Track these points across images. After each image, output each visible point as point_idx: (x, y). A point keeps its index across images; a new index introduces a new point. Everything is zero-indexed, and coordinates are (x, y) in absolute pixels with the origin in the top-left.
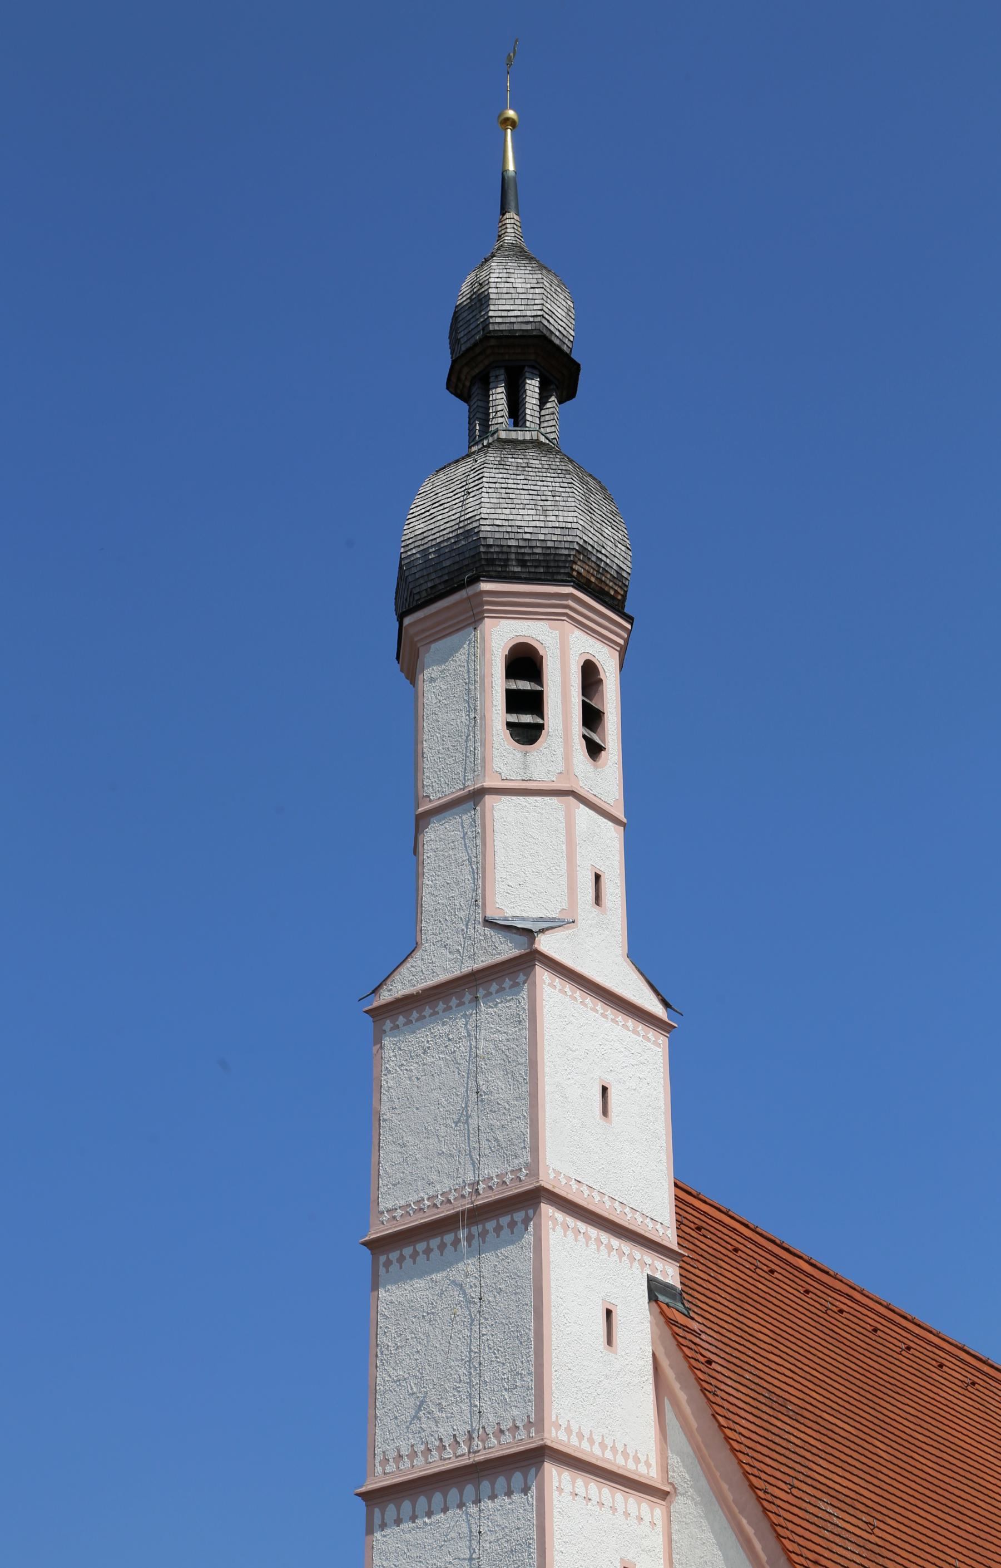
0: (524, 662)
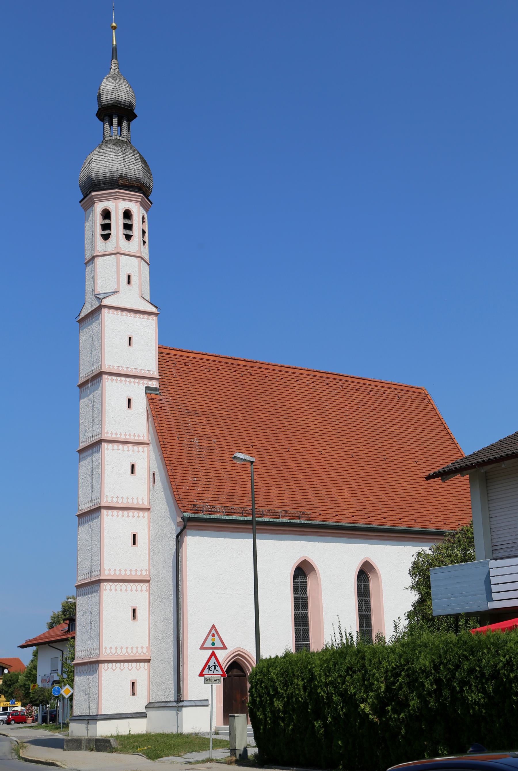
0: (106, 214)
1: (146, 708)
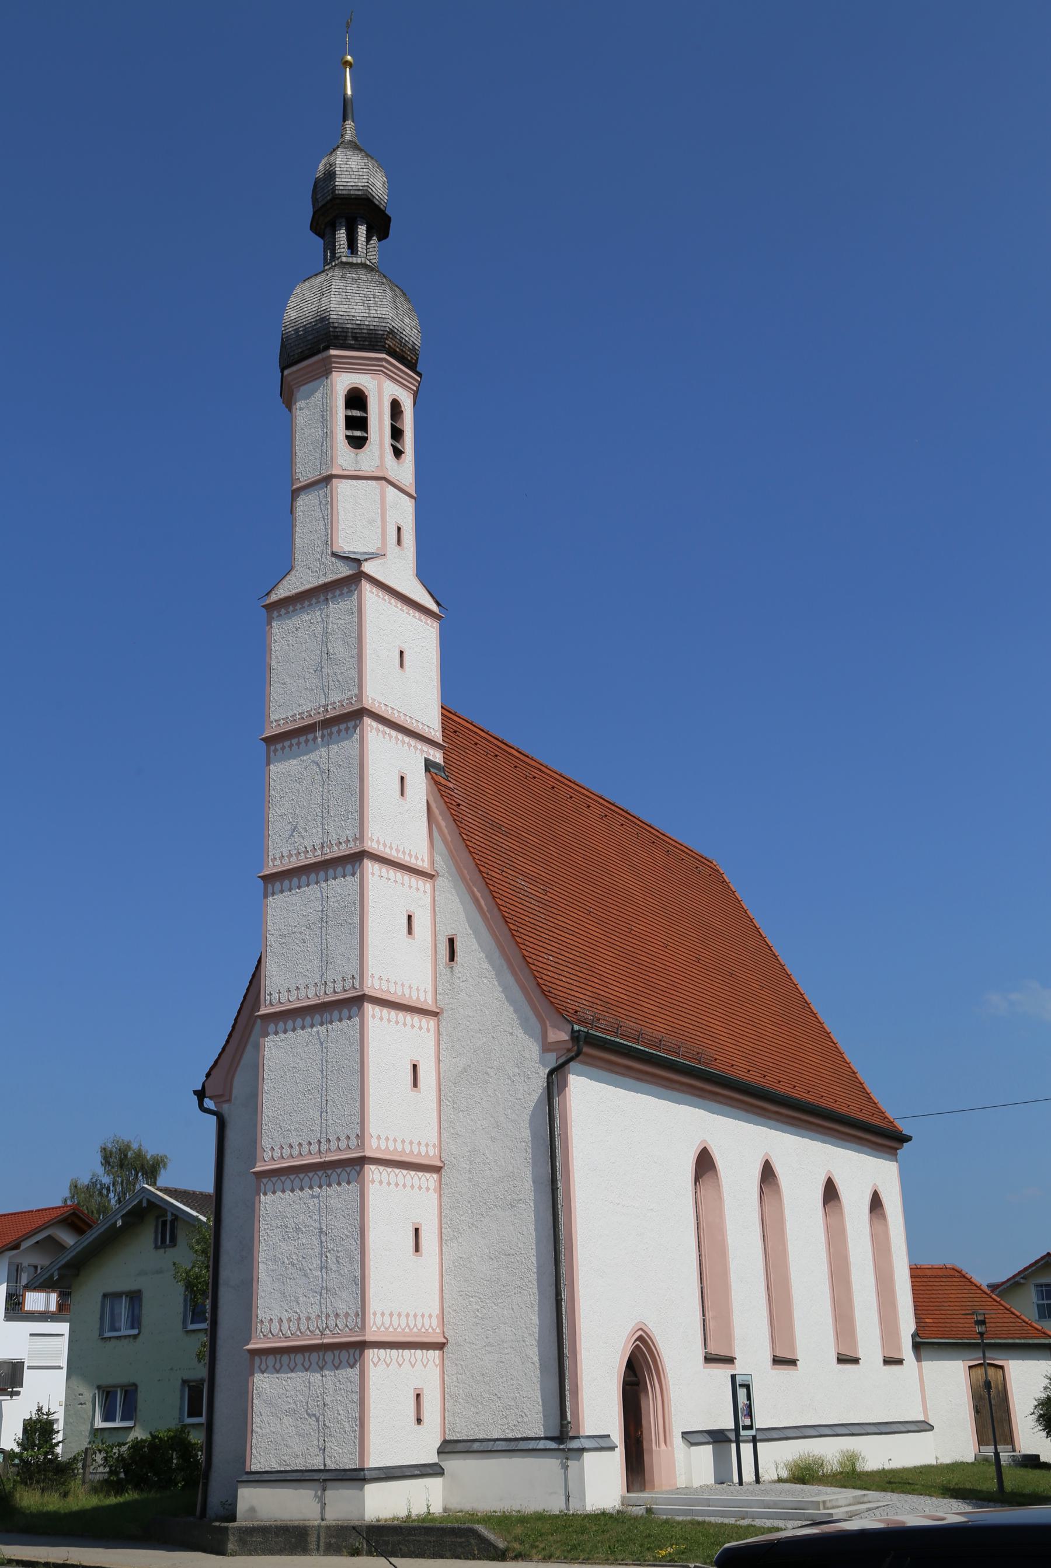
0: (356, 399)
1: (439, 1453)
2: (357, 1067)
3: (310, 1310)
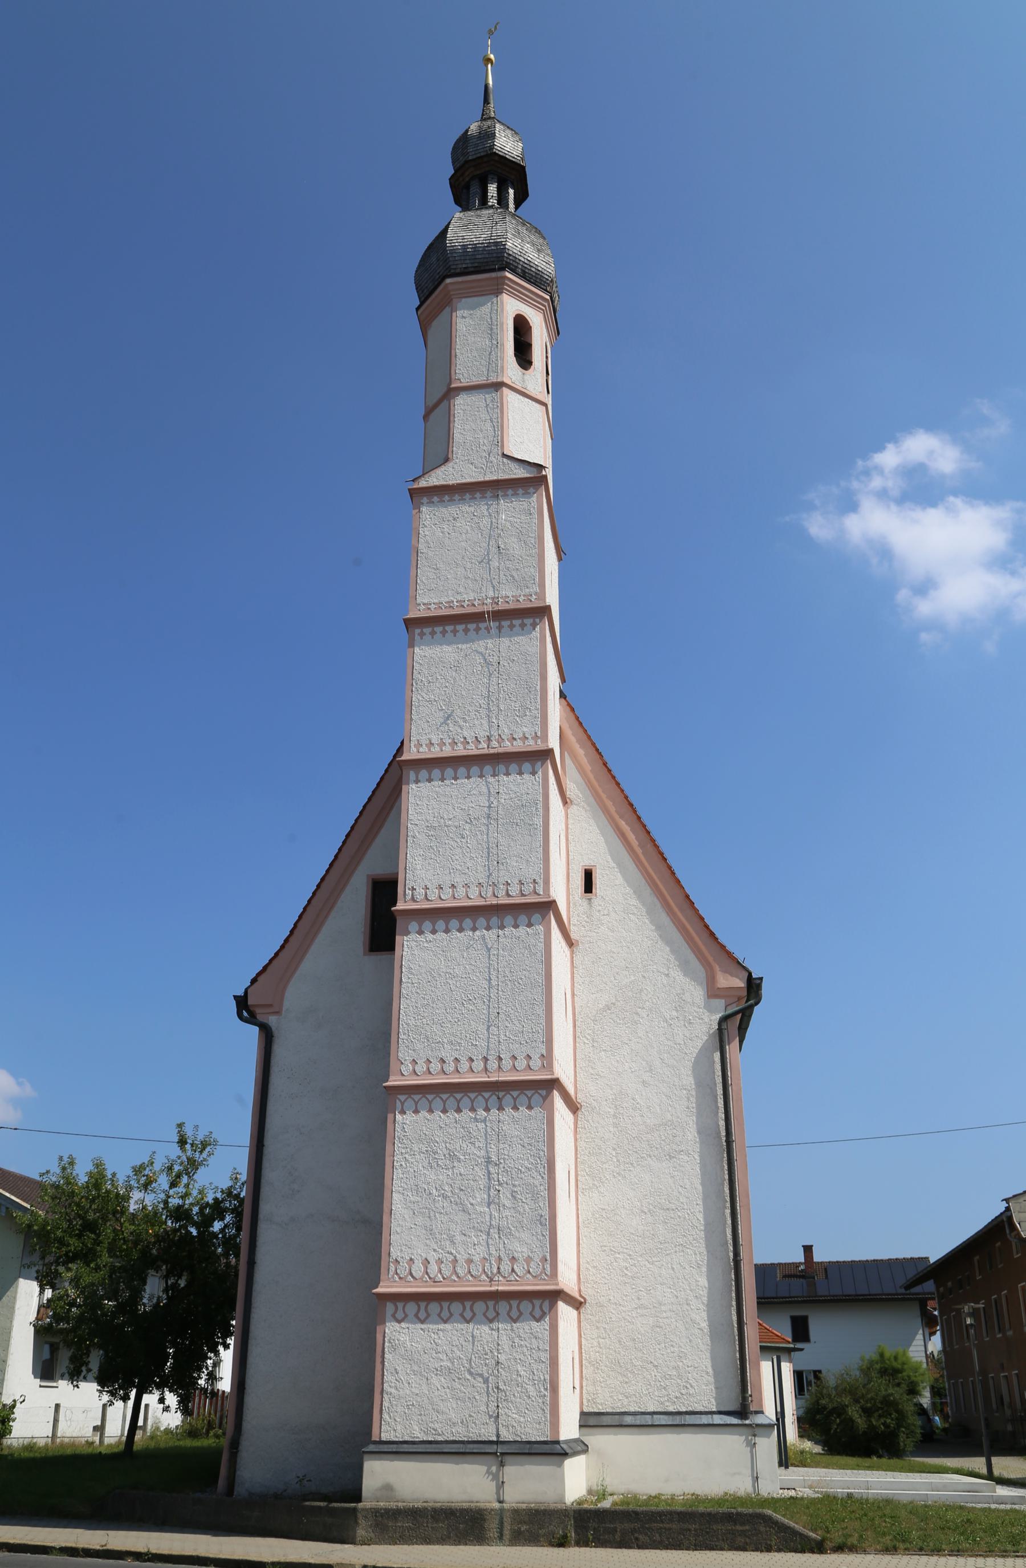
2: (541, 980)
3: (472, 1251)
